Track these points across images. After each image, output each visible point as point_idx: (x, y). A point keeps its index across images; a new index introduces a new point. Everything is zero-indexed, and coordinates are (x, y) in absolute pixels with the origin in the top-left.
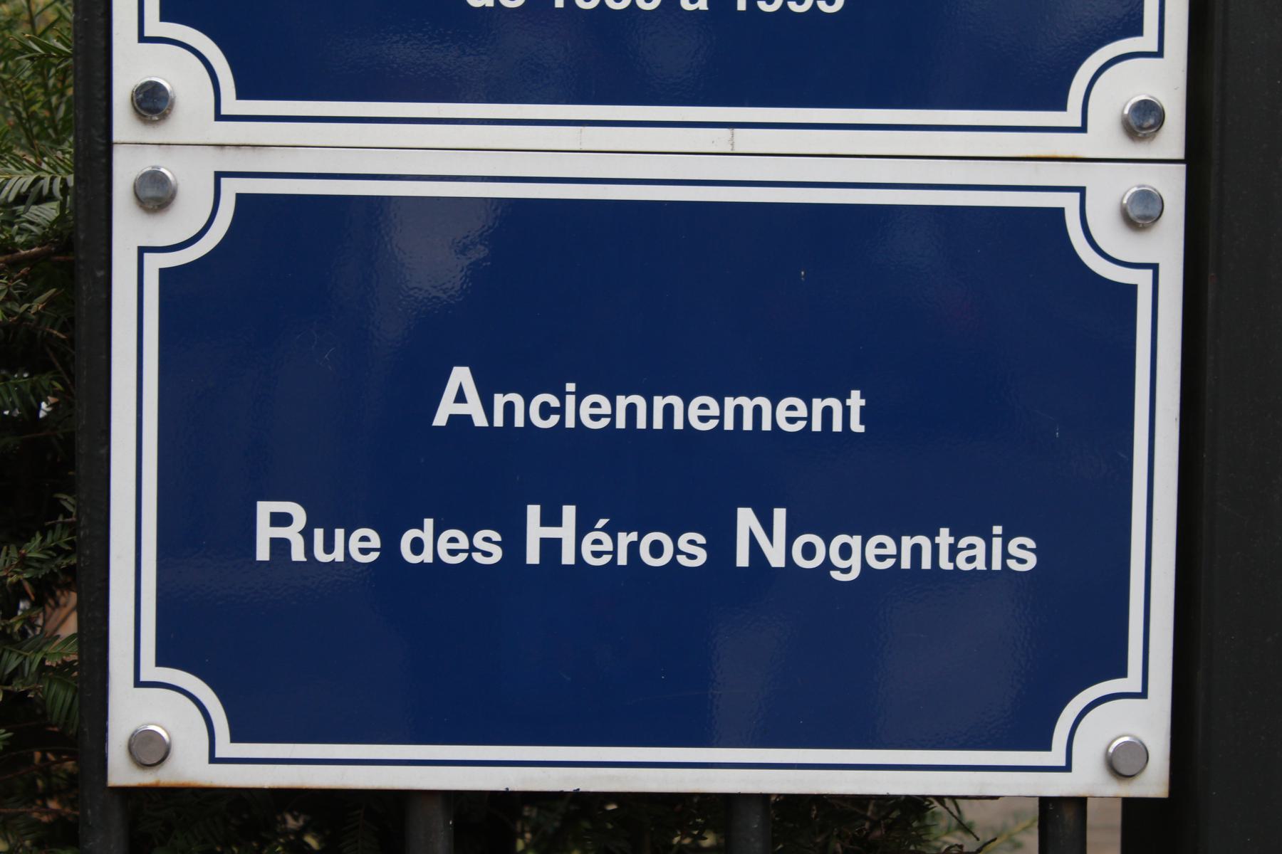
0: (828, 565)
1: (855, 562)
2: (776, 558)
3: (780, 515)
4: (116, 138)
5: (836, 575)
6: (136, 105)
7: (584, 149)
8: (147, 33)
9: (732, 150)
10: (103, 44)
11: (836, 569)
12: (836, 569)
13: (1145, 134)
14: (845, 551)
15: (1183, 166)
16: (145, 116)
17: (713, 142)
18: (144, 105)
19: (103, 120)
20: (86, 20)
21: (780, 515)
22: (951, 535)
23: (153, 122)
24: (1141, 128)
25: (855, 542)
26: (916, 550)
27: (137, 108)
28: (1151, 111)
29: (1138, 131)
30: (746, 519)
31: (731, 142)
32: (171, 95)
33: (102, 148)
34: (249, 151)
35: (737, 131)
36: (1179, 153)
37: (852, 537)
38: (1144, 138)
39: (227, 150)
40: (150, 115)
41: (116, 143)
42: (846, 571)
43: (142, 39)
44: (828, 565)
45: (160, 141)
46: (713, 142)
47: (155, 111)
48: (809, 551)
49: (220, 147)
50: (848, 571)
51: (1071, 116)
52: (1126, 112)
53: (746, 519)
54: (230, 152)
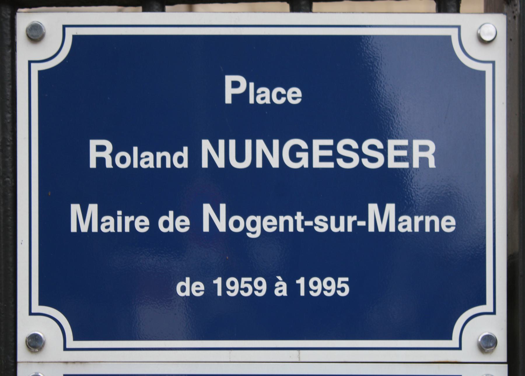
0: (245, 230)
1: (258, 228)
2: (221, 227)
3: (223, 207)
4: (19, 359)
5: (249, 235)
6: (28, 345)
7: (231, 361)
8: (33, 311)
9: (299, 360)
10: (13, 316)
11: (249, 232)
12: (249, 232)
13: (488, 351)
14: (254, 224)
15: (506, 365)
16: (31, 349)
17: (290, 357)
18: (31, 345)
19: (13, 352)
20: (5, 305)
21: (223, 207)
22: (302, 215)
23: (35, 352)
24: (487, 347)
25: (258, 219)
26: (286, 223)
27: (28, 346)
28: (491, 340)
29: (485, 349)
30: (207, 209)
31: (298, 357)
32: (44, 339)
33: (12, 364)
34: (79, 364)
35: (301, 351)
36: (505, 360)
37: (256, 217)
38: (487, 353)
39: (69, 364)
40: (34, 349)
41: (19, 362)
42: (254, 233)
43: (31, 314)
44: (245, 230)
45: (39, 361)
46: (290, 357)
47: (35, 347)
48: (237, 224)
49: (66, 363)
50: (255, 233)
51: (454, 342)
52: (480, 340)
53: (207, 209)
54: (70, 365)
